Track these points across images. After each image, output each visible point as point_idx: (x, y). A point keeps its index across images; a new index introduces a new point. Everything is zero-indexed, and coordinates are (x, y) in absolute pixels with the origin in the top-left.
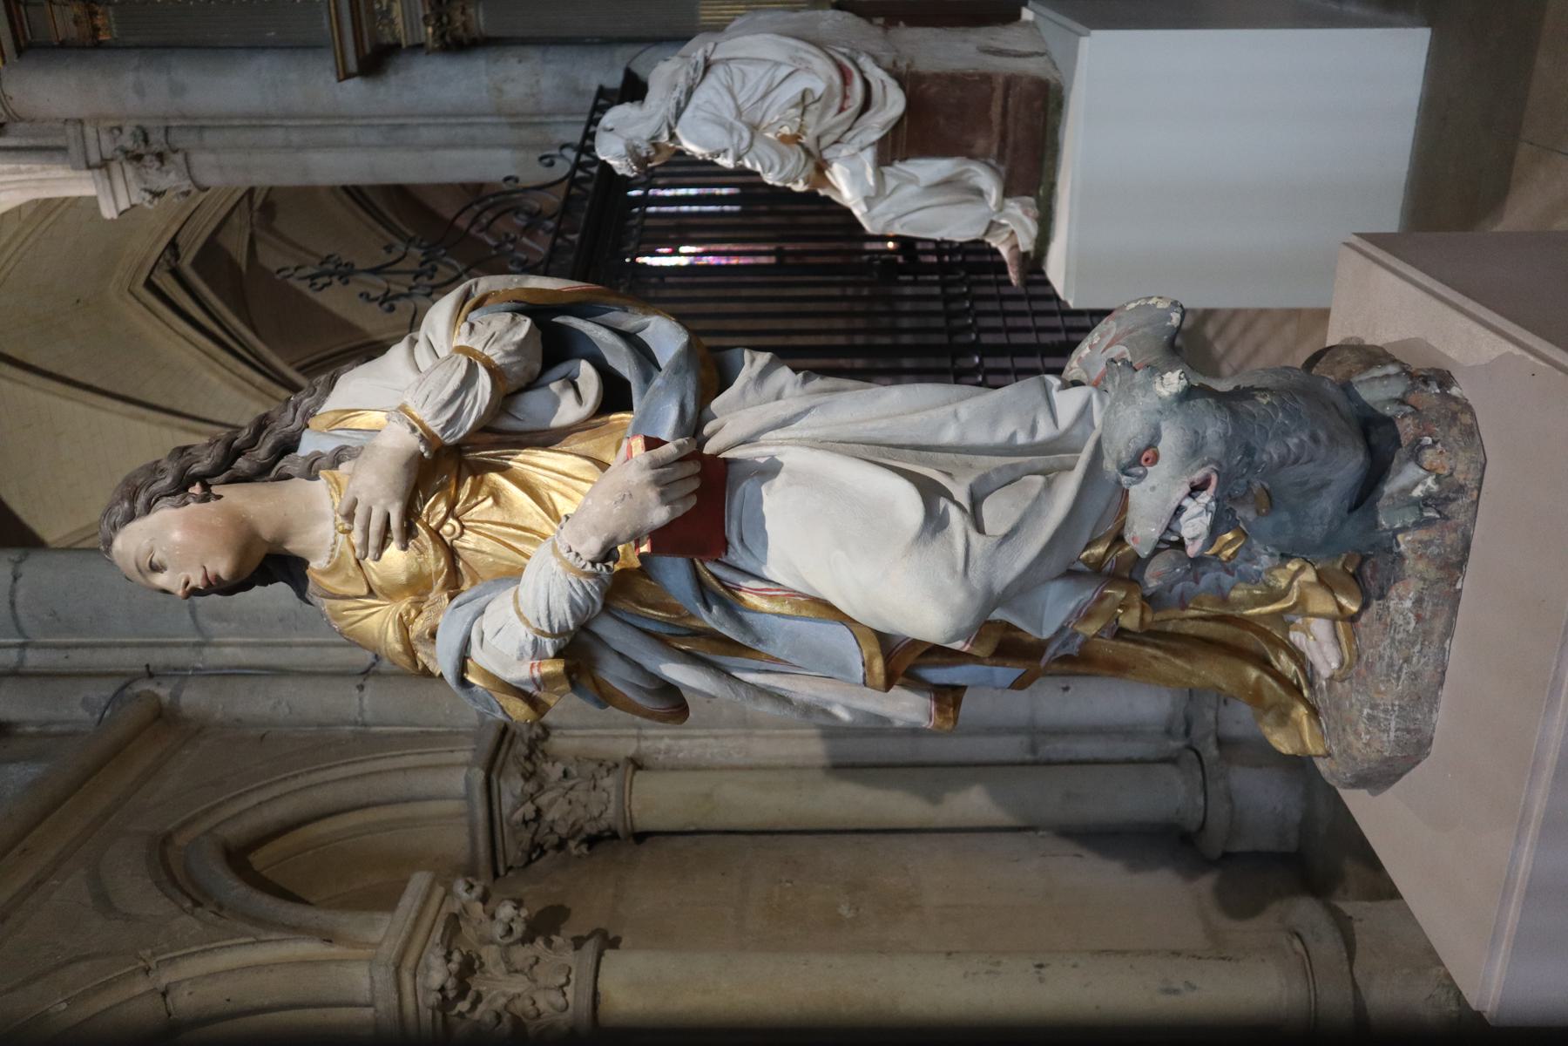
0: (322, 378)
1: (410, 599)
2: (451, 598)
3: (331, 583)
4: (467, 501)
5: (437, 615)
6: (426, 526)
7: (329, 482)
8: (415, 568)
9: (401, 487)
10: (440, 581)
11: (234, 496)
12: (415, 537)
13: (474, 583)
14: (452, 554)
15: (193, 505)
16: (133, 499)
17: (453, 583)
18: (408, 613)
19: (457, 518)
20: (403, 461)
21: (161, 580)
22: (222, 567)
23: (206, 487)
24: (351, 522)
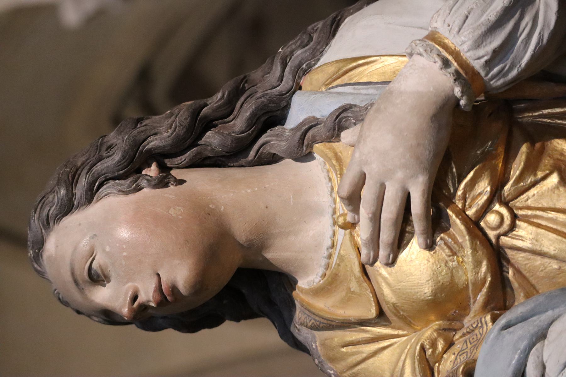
0: (320, 25)
1: (437, 324)
2: (494, 319)
3: (326, 306)
4: (520, 178)
5: (476, 347)
6: (461, 214)
7: (327, 159)
8: (444, 277)
9: (426, 153)
10: (481, 298)
11: (201, 182)
12: (445, 230)
13: (528, 296)
14: (498, 256)
15: (147, 191)
16: (72, 183)
17: (500, 298)
18: (434, 345)
19: (506, 204)
20: (430, 110)
21: (102, 296)
22: (180, 274)
23: (163, 168)
24: (356, 210)
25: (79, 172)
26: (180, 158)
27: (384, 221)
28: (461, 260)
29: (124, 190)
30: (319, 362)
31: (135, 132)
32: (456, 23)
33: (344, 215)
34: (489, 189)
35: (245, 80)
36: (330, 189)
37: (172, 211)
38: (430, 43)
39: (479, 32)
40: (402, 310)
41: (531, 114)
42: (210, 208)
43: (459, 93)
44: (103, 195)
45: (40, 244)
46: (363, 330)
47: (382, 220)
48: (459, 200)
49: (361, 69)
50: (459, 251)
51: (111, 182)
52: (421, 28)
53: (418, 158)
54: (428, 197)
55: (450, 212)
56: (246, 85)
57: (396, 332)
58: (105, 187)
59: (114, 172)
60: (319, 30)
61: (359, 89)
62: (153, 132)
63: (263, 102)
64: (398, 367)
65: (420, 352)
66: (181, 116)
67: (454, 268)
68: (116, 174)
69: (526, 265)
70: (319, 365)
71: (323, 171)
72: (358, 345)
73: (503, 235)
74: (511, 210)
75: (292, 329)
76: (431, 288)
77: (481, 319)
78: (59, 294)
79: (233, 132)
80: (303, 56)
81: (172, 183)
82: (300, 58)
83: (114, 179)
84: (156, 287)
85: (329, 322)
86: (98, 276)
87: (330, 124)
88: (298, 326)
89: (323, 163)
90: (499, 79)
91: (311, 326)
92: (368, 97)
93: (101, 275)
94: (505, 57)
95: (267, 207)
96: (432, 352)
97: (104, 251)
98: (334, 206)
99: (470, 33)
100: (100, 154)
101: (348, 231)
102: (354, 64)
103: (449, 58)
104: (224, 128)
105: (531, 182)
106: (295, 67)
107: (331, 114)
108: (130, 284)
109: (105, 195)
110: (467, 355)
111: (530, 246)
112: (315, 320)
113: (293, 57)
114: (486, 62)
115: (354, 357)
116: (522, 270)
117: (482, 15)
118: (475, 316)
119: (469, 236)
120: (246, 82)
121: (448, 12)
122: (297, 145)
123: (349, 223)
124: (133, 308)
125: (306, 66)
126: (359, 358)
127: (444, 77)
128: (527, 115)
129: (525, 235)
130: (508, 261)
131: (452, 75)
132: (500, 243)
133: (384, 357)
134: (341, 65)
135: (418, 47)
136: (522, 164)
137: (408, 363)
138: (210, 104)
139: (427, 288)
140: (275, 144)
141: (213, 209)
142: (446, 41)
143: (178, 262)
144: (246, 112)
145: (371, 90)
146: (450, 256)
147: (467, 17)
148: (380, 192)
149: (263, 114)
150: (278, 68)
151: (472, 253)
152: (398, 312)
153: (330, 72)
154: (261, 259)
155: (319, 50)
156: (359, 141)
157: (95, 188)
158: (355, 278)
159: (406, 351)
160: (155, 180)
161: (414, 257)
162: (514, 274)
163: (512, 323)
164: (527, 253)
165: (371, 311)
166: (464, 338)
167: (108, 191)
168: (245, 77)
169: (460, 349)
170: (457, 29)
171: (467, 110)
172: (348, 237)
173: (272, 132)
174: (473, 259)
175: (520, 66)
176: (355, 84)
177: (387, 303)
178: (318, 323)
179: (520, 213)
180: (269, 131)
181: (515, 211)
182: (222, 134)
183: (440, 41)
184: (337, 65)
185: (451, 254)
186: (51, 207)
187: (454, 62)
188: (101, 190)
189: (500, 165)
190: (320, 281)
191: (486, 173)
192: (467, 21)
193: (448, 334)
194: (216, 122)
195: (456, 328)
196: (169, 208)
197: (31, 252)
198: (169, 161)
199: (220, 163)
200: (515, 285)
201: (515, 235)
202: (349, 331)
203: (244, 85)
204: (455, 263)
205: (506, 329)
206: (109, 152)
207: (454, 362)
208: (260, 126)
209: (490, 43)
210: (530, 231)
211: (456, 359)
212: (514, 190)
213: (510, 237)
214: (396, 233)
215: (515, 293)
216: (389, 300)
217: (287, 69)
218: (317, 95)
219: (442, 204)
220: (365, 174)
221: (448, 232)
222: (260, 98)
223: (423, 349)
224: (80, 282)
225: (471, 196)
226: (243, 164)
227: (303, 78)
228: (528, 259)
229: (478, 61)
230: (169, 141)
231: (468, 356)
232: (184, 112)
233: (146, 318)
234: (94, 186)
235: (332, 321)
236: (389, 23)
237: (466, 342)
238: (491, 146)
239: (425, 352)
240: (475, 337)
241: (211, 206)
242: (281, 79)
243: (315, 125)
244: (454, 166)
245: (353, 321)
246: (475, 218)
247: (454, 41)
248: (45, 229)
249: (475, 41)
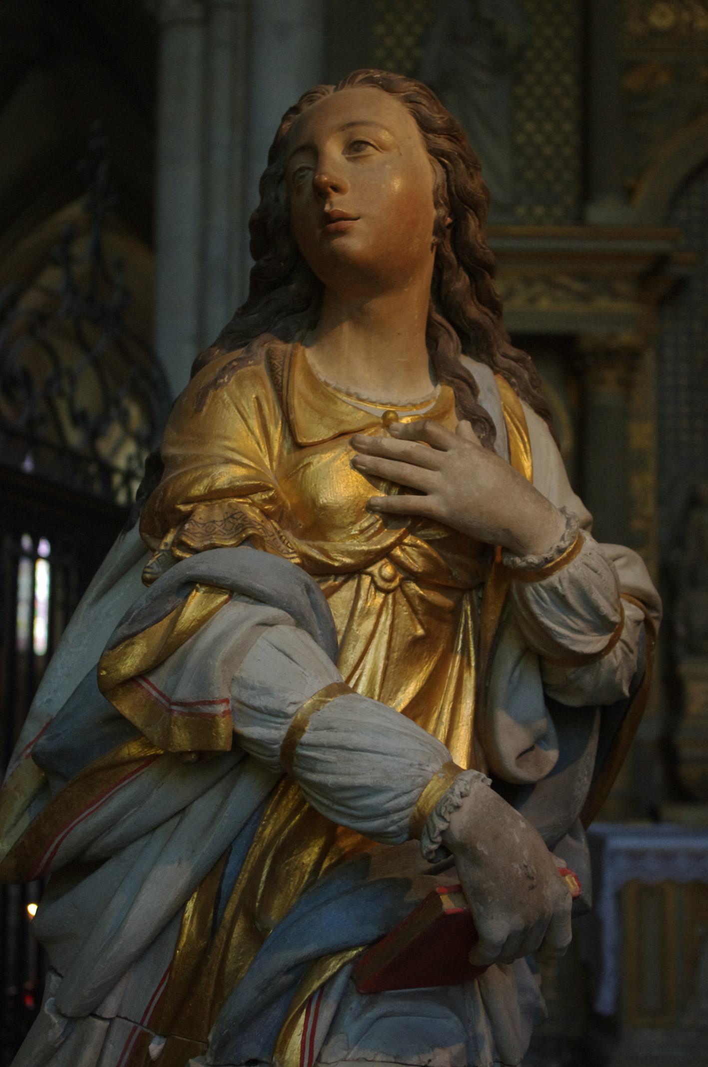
6: (399, 542)
12: (385, 525)
16: (451, 133)
30: (234, 367)
32: (593, 562)
39: (584, 583)
45: (388, 88)
47: (407, 465)
68: (452, 183)
70: (230, 367)
74: (393, 590)
86: (358, 151)
90: (533, 596)
101: (382, 421)
112: (283, 370)
123: (391, 423)
137: (240, 472)
170: (588, 562)
172: (376, 420)
178: (280, 373)
179: (390, 596)
186: (428, 108)
217: (513, 363)
220: (445, 450)
224: (351, 130)
242: (505, 356)
245: (292, 417)
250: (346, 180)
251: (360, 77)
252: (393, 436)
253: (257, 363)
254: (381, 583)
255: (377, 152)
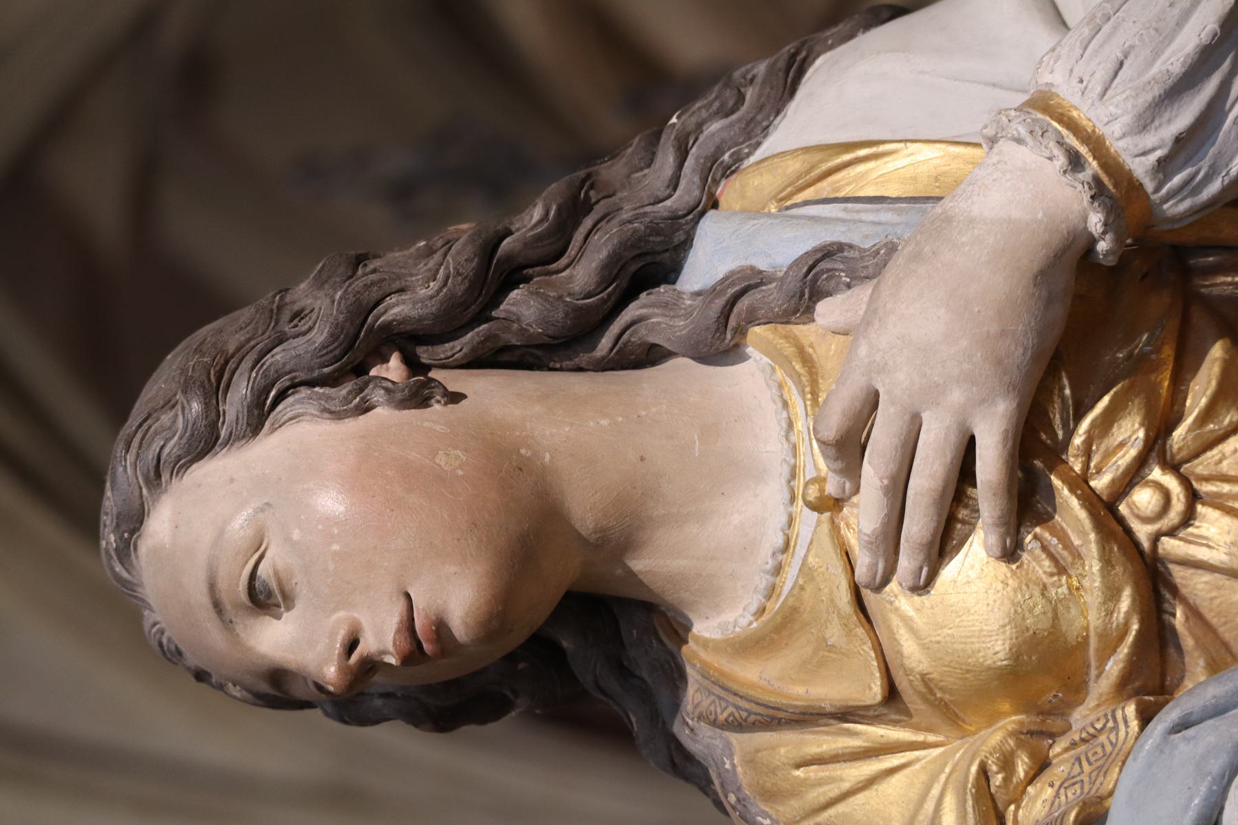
1: (1012, 721)
2: (1146, 718)
3: (764, 676)
4: (1208, 414)
5: (1103, 770)
6: (1080, 484)
8: (1037, 619)
9: (1017, 352)
10: (1115, 666)
11: (495, 396)
12: (1044, 518)
13: (1214, 668)
14: (1153, 579)
15: (383, 413)
17: (1153, 675)
18: (1007, 765)
19: (1174, 467)
20: (1033, 260)
21: (274, 639)
22: (457, 596)
23: (414, 365)
25: (231, 365)
26: (451, 344)
27: (916, 494)
28: (1075, 583)
29: (333, 409)
30: (739, 800)
31: (358, 284)
32: (1098, 76)
33: (819, 480)
34: (1141, 434)
35: (589, 181)
36: (784, 425)
37: (441, 459)
38: (1040, 116)
39: (1148, 97)
40: (941, 689)
41: (1229, 279)
42: (522, 456)
43: (1099, 225)
44: (286, 418)
45: (134, 520)
46: (848, 730)
47: (910, 492)
48: (1076, 456)
49: (861, 168)
50: (1073, 564)
51: (304, 392)
52: (994, 85)
53: (999, 362)
54: (1014, 446)
55: (1056, 482)
56: (592, 193)
57: (920, 737)
58: (290, 400)
59: (311, 369)
60: (759, 80)
61: (858, 211)
62: (397, 285)
63: (635, 231)
64: (923, 812)
65: (977, 779)
66: (458, 253)
67: (1060, 601)
68: (316, 373)
69: (1212, 599)
70: (739, 807)
71: (767, 385)
72: (832, 762)
73: (1166, 534)
74: (1185, 482)
75: (677, 728)
76: (1008, 642)
77: (1114, 712)
78: (163, 633)
79: (569, 294)
80: (725, 135)
81: (438, 397)
82: (717, 140)
83: (311, 384)
84: (401, 622)
85: (771, 712)
86: (270, 594)
87: (793, 285)
88: (690, 722)
89: (768, 369)
91: (726, 720)
92: (879, 229)
93: (277, 592)
94: (1197, 152)
95: (642, 459)
96: (1005, 779)
97: (287, 539)
98: (793, 461)
99: (1127, 98)
100: (278, 329)
101: (828, 514)
102: (847, 157)
103: (1084, 151)
104: (548, 284)
105: (1231, 423)
106: (706, 158)
107: (797, 262)
108: (341, 614)
109: (291, 419)
110: (1082, 788)
111: (1224, 558)
112: (738, 708)
113: (701, 139)
114: (1160, 161)
115: (821, 790)
116: (1204, 611)
117: (1154, 60)
118: (1098, 706)
119: (1097, 533)
120: (592, 187)
121: (1078, 51)
122: (715, 327)
123: (829, 497)
124: (349, 667)
125: (731, 156)
126: (833, 791)
127: (1069, 191)
128: (1222, 279)
129: (1215, 534)
130: (1174, 590)
131: (1086, 187)
132: (1160, 551)
133: (890, 791)
134: (817, 156)
135: (1014, 125)
136: (1214, 383)
137: (950, 802)
138: (518, 230)
139: (1000, 642)
140: (659, 323)
141: (529, 459)
142: (1075, 114)
143: (453, 569)
144: (598, 252)
145: (886, 215)
146: (1052, 575)
147: (1121, 64)
148: (909, 432)
149: (633, 258)
150: (666, 159)
151: (1102, 570)
152: (931, 691)
153: (790, 170)
154: (619, 572)
155: (760, 123)
156: (867, 322)
157: (268, 402)
158: (840, 617)
159: (943, 777)
160: (403, 390)
161: (973, 574)
162: (1187, 619)
163: (1193, 718)
164: (1217, 575)
165: (870, 689)
166: (1072, 752)
167: (299, 409)
168: (589, 176)
169: (1065, 775)
170: (1099, 89)
171: (1113, 264)
172: (825, 527)
173: (652, 297)
174: (1102, 582)
175: (1227, 174)
176: (846, 200)
177: (908, 672)
178: (744, 714)
179: (1205, 488)
180: (643, 295)
181: (1194, 483)
182: (546, 298)
183: (1062, 115)
184: (806, 157)
185: (1055, 570)
186: (167, 440)
187: (1091, 159)
188: (280, 407)
189: (1166, 384)
190: (751, 623)
191: (1137, 401)
192: (1121, 73)
193: (1037, 742)
194: (530, 271)
195: (1054, 730)
196: (434, 453)
197: (112, 538)
198: (425, 351)
199: (531, 360)
200: (1188, 642)
201: (1192, 535)
202: (812, 733)
203: (587, 193)
204: (1064, 590)
205: (1180, 731)
206: (296, 326)
207: (1053, 804)
208: (624, 282)
209: (1169, 121)
210: (1227, 528)
211: (1057, 795)
212: (1194, 439)
213: (1181, 539)
214: (939, 522)
215: (1187, 659)
216: (914, 665)
217: (690, 163)
218: (762, 221)
219: (1038, 463)
220: (877, 394)
221: (1050, 523)
222: (630, 222)
223: (984, 772)
224: (228, 607)
225: (1103, 448)
226: (583, 365)
227: (723, 183)
228: (1219, 588)
229: (1143, 158)
230: (432, 307)
231: (1086, 789)
232: (464, 245)
233: (362, 694)
234: (266, 399)
235: (778, 709)
236: (922, 72)
237: (1079, 760)
238: (1148, 343)
239: (988, 779)
240: (1099, 750)
241: (523, 451)
242: (674, 183)
243: (756, 286)
244: (1066, 382)
245: (829, 709)
246: (1110, 495)
247: (1091, 115)
248: (149, 489)
249: (1140, 117)
250: (335, 627)
251: (118, 568)
252: (857, 490)
253: (729, 749)
254: (1174, 516)
255: (268, 554)
